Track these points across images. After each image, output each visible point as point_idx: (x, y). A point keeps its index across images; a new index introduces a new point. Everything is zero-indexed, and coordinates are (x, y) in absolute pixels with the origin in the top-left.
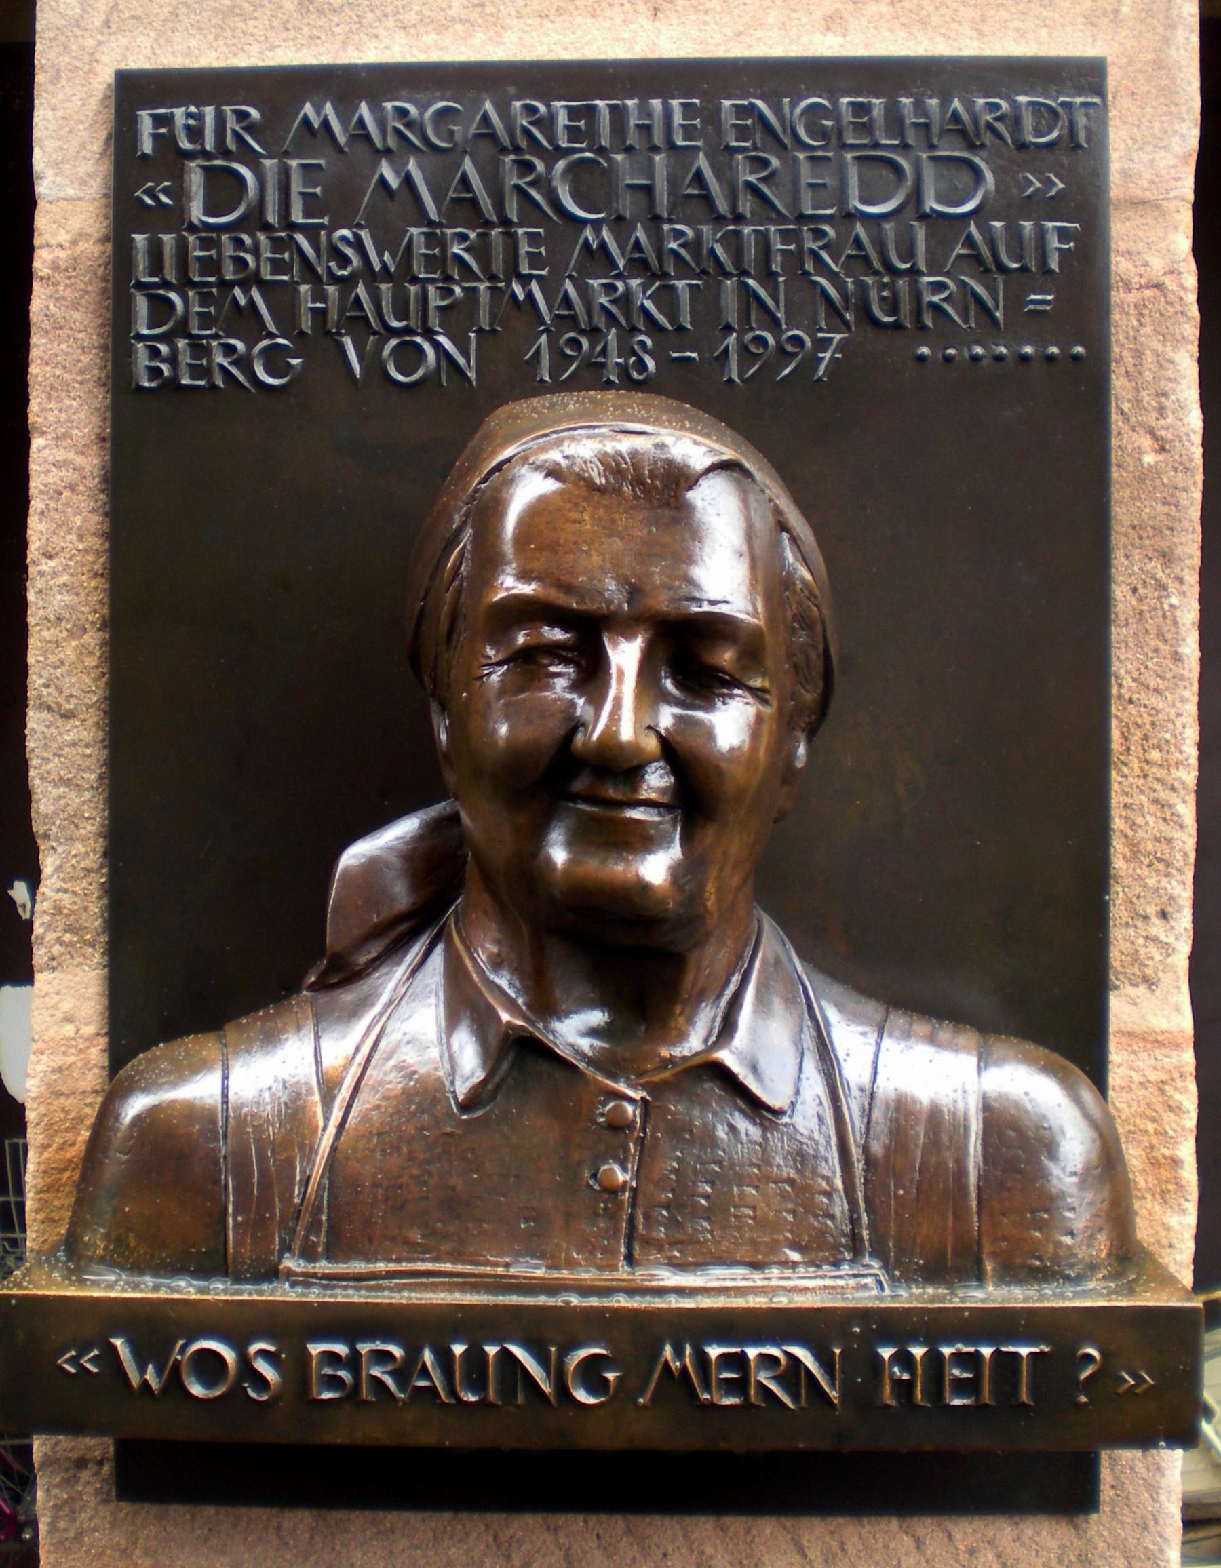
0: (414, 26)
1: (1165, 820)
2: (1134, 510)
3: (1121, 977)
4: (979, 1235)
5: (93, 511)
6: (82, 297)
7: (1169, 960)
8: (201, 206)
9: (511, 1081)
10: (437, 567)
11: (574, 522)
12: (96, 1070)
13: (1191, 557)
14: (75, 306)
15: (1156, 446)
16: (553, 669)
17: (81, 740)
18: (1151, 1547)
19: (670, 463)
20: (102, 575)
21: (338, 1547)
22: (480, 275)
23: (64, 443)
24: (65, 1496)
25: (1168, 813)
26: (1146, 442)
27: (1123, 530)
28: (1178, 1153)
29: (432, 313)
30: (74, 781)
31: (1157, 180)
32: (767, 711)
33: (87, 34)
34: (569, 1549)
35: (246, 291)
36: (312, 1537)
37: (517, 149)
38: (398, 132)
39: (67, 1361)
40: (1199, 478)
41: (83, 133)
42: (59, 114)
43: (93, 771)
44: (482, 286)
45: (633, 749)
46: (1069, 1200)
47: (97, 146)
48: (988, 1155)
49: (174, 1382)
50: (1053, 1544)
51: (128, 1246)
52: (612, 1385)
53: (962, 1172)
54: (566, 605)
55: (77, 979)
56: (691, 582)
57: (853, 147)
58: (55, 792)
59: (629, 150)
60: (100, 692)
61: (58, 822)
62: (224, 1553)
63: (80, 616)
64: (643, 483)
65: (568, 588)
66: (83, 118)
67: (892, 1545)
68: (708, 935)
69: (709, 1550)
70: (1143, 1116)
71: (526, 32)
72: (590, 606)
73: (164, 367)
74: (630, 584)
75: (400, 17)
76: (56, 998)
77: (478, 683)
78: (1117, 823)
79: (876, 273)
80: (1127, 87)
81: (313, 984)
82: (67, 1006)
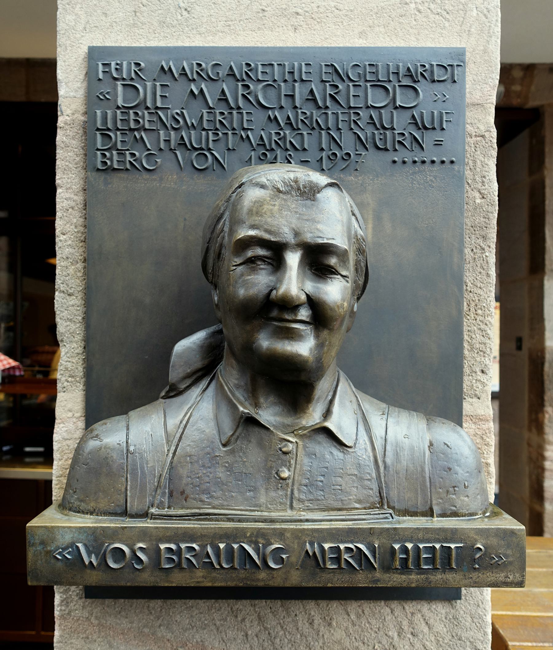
0: (204, 33)
1: (483, 336)
2: (472, 220)
5: (81, 217)
6: (76, 135)
10: (214, 228)
12: (80, 430)
13: (493, 238)
14: (73, 138)
15: (481, 197)
18: (481, 613)
21: (171, 614)
24: (65, 596)
25: (484, 334)
26: (477, 195)
28: (488, 461)
29: (211, 142)
30: (74, 320)
33: (77, 32)
34: (259, 613)
35: (139, 133)
36: (161, 610)
38: (197, 72)
40: (497, 208)
41: (77, 72)
43: (80, 316)
44: (230, 133)
45: (298, 298)
47: (82, 77)
50: (443, 612)
52: (285, 560)
53: (423, 470)
54: (269, 239)
55: (73, 395)
57: (370, 81)
58: (65, 324)
59: (285, 81)
60: (83, 286)
61: (67, 335)
62: (127, 618)
63: (76, 257)
67: (382, 611)
69: (313, 613)
76: (65, 402)
78: (466, 337)
79: (378, 129)
80: (472, 60)
81: (164, 396)
82: (69, 406)
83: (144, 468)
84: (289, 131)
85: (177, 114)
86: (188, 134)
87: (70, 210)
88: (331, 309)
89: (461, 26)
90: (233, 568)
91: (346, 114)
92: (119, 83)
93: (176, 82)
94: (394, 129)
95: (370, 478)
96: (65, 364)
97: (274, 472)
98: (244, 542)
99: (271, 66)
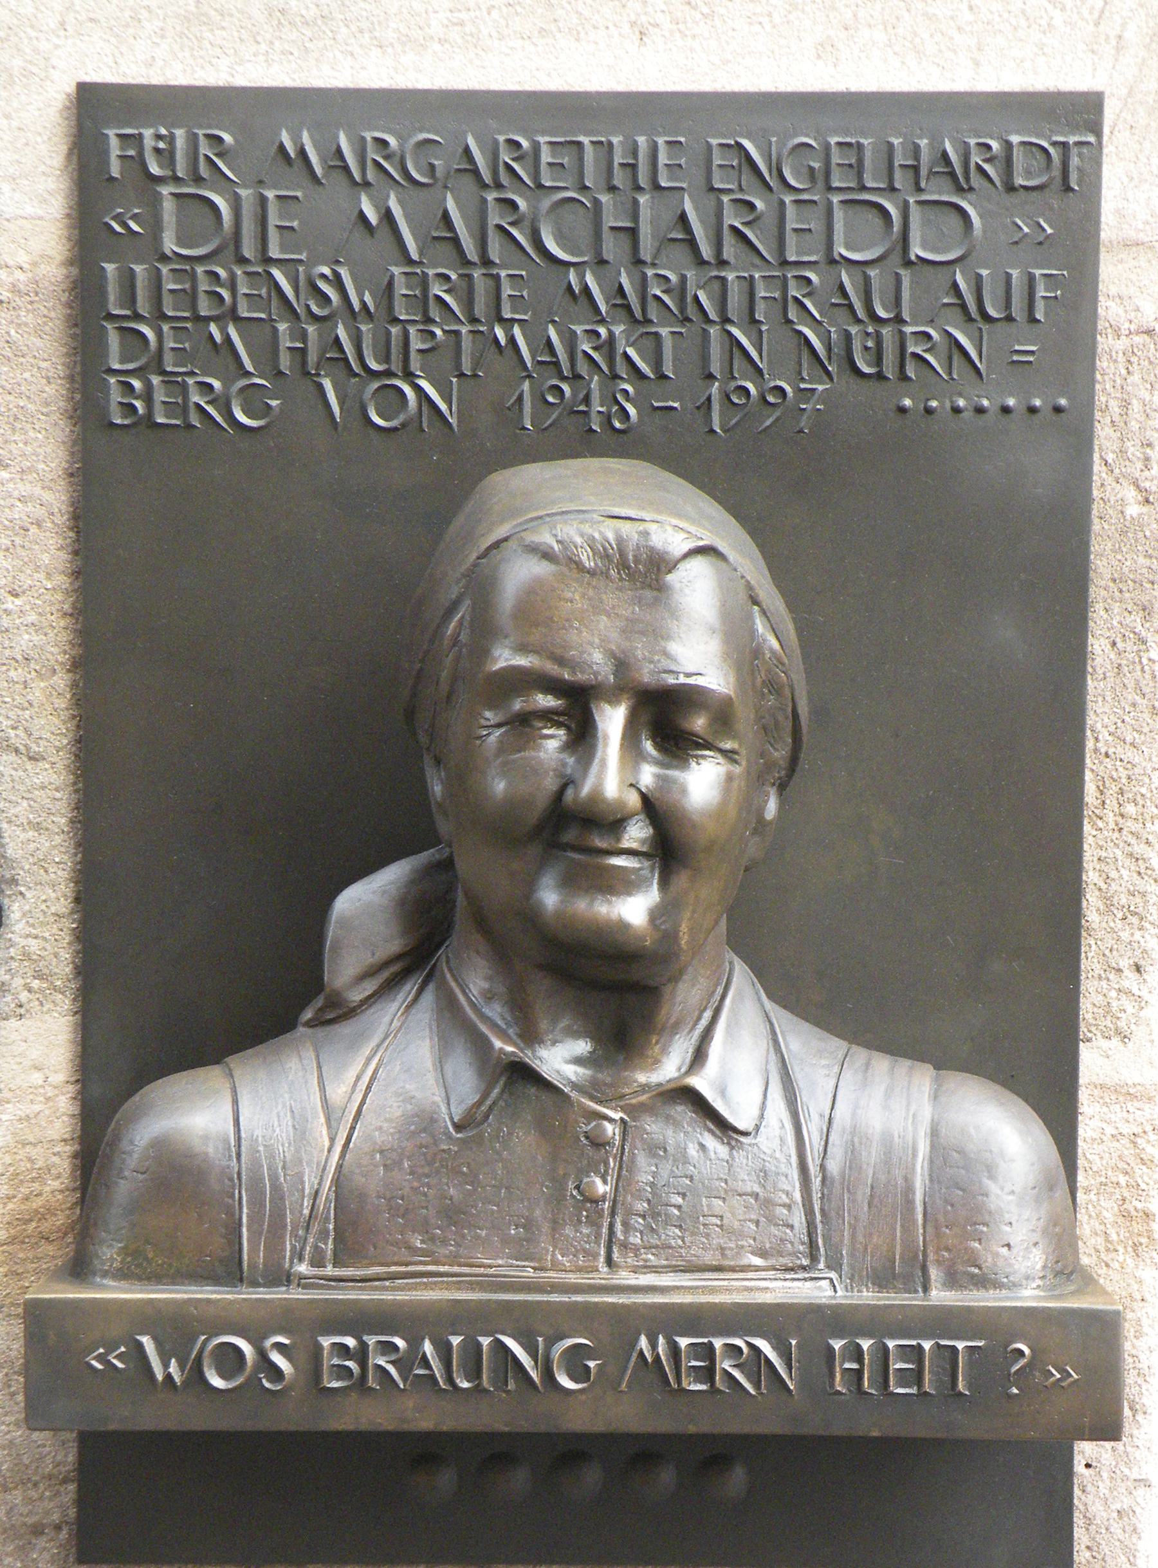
1: (1139, 873)
3: (1093, 1029)
4: (924, 1246)
5: (61, 548)
6: (45, 324)
7: (1142, 1013)
8: (174, 236)
9: (501, 1103)
11: (567, 601)
12: (65, 1118)
16: (546, 731)
17: (51, 783)
19: (652, 549)
20: (71, 615)
22: (463, 320)
23: (30, 478)
26: (1131, 494)
27: (1103, 583)
29: (413, 355)
31: (1151, 220)
32: (737, 770)
37: (499, 186)
39: (94, 1358)
42: (15, 124)
45: (620, 803)
46: (1007, 1216)
48: (934, 1177)
49: (197, 1376)
51: (146, 1259)
53: (909, 1190)
56: (666, 654)
59: (612, 189)
60: (71, 735)
64: (629, 568)
65: (561, 661)
66: (40, 130)
68: (681, 972)
70: (1115, 1168)
71: (507, 55)
72: (581, 677)
73: (138, 404)
74: (615, 658)
75: (377, 34)
77: (478, 742)
79: (859, 321)
81: (310, 1020)
82: (35, 1054)
83: (277, 1179)
84: (622, 327)
85: (323, 276)
86: (354, 331)
87: (34, 530)
88: (694, 826)
89: (1097, 24)
90: (478, 1389)
91: (776, 281)
92: (165, 190)
93: (320, 189)
94: (904, 322)
95: (788, 1201)
96: (23, 942)
97: (571, 1185)
98: (503, 1333)
99: (575, 147)
